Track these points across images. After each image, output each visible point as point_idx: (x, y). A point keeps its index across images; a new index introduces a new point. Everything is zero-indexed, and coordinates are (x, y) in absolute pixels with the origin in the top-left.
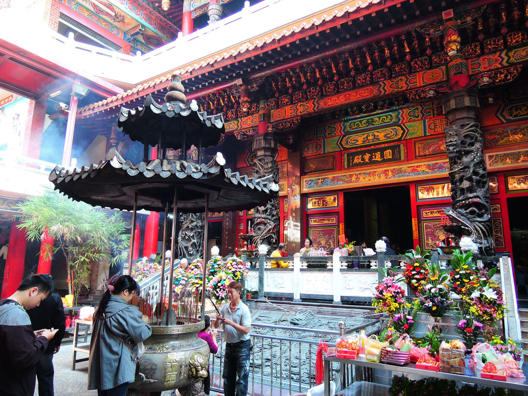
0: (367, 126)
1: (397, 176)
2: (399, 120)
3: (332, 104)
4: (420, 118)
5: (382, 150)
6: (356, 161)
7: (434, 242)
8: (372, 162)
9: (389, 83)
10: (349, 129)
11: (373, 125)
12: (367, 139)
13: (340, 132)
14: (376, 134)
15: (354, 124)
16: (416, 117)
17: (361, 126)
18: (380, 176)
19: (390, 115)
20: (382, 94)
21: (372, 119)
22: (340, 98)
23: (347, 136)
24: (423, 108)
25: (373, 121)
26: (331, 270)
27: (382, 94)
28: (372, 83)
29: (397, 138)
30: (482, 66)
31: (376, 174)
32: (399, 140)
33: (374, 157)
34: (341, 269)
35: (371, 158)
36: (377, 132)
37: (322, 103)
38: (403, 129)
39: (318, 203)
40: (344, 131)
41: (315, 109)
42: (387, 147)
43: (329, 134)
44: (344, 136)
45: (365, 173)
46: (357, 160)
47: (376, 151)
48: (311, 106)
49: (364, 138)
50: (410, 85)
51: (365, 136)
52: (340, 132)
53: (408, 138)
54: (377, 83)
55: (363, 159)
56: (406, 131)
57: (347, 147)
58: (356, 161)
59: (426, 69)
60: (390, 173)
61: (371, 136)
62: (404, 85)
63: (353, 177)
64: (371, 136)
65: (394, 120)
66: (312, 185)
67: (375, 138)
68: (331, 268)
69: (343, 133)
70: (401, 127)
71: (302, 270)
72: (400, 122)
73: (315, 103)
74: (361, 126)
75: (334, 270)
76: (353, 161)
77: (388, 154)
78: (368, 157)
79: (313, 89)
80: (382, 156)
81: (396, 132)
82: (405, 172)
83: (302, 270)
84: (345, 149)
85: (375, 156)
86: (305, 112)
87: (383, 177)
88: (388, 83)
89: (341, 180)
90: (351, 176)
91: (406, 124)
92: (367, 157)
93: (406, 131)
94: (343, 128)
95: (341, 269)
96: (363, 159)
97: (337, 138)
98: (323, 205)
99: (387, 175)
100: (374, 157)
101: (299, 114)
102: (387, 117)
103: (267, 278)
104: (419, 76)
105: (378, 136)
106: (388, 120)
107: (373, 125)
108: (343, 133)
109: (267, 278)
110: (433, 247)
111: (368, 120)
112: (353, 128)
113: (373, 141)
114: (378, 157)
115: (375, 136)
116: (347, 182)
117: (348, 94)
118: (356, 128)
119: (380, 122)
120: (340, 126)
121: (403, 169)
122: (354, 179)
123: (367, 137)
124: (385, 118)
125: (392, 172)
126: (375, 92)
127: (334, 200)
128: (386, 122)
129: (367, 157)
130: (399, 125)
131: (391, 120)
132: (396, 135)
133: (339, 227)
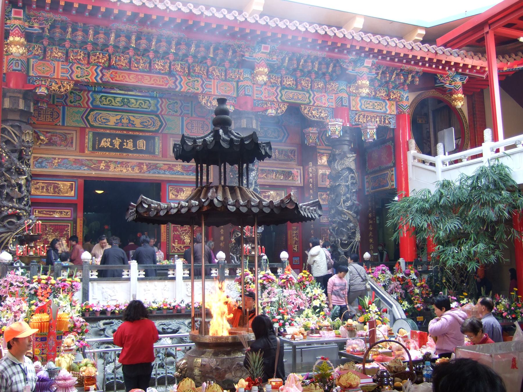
0: (122, 106)
1: (152, 171)
2: (158, 109)
3: (121, 81)
4: (178, 113)
5: (135, 138)
6: (103, 144)
7: (180, 245)
8: (122, 149)
9: (186, 80)
10: (98, 103)
11: (129, 107)
12: (121, 122)
13: (87, 103)
14: (132, 118)
15: (106, 99)
16: (174, 111)
17: (113, 104)
18: (133, 169)
19: (148, 101)
20: (177, 90)
21: (128, 99)
22: (131, 77)
23: (96, 112)
24: (182, 104)
25: (129, 102)
26: (174, 279)
27: (177, 90)
28: (170, 73)
29: (154, 129)
30: (263, 95)
31: (130, 165)
32: (156, 132)
33: (125, 144)
34: (183, 277)
35: (121, 145)
36: (133, 116)
37: (108, 75)
38: (160, 121)
39: (47, 190)
40: (92, 103)
41: (98, 78)
42: (141, 136)
43: (71, 102)
44: (92, 110)
45: (116, 162)
46: (105, 143)
47: (128, 137)
48: (93, 74)
49: (117, 120)
50: (206, 90)
51: (118, 117)
52: (87, 103)
53: (166, 132)
54: (174, 76)
55: (112, 144)
56: (164, 124)
57: (95, 124)
58: (103, 144)
59: (222, 80)
60: (145, 167)
61: (125, 119)
62: (200, 88)
63: (102, 164)
64: (125, 119)
65: (152, 108)
66: (44, 165)
67: (130, 122)
68: (173, 276)
69: (91, 107)
70: (159, 118)
71: (140, 279)
72: (159, 113)
73: (98, 71)
74: (113, 104)
75: (177, 279)
76: (100, 143)
77: (141, 144)
78: (118, 143)
79: (100, 54)
80: (135, 145)
81: (154, 122)
82: (160, 169)
83: (140, 279)
84: (92, 127)
85: (127, 143)
86: (84, 79)
87: (136, 170)
88: (185, 80)
89: (86, 166)
90: (100, 162)
91: (164, 116)
92: (117, 142)
93: (164, 124)
94: (91, 99)
95: (183, 277)
96: (112, 144)
97: (82, 110)
98: (55, 192)
99: (141, 169)
100: (125, 144)
101: (75, 78)
102: (145, 103)
103: (93, 290)
104: (214, 83)
105: (133, 121)
106: (145, 107)
107: (129, 107)
108: (91, 107)
109: (93, 290)
110: (178, 250)
111: (123, 99)
112: (105, 103)
113: (127, 126)
114: (130, 145)
115: (130, 120)
116: (93, 169)
117: (141, 75)
118: (108, 105)
119: (137, 106)
120: (87, 95)
121: (158, 165)
122: (102, 166)
123: (121, 119)
124: (143, 103)
125: (147, 165)
126: (171, 85)
127: (71, 187)
128: (143, 108)
129: (117, 142)
130: (157, 116)
131: (150, 107)
132: (153, 125)
133: (75, 222)
